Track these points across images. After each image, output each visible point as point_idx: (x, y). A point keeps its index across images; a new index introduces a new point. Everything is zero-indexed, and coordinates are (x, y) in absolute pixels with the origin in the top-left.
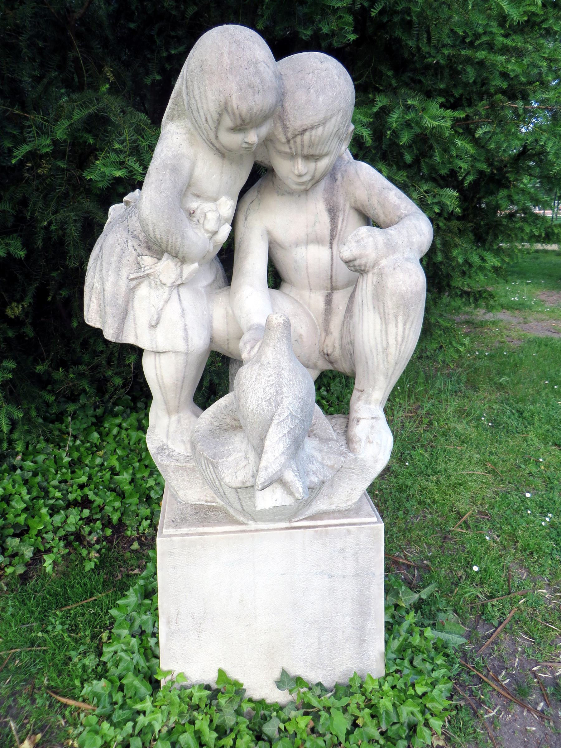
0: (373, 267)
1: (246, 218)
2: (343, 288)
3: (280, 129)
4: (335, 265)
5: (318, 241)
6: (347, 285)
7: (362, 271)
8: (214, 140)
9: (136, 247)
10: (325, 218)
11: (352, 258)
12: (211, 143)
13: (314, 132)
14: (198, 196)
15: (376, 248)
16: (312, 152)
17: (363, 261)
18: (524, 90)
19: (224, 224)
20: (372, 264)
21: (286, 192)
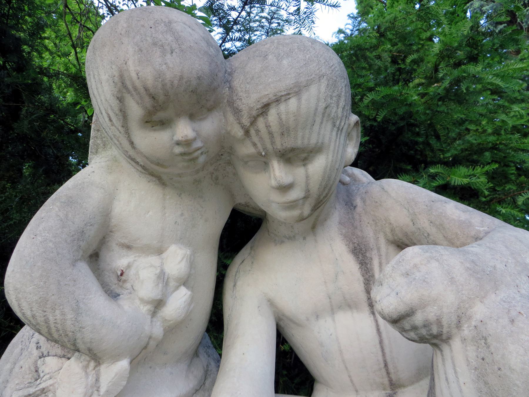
0: (459, 325)
1: (234, 286)
2: (412, 383)
3: (231, 118)
4: (386, 342)
5: (348, 305)
6: (417, 377)
7: (433, 338)
8: (132, 152)
10: (350, 265)
11: (402, 309)
12: (130, 157)
13: (282, 107)
14: (128, 247)
15: (452, 280)
16: (289, 143)
17: (430, 313)
19: (177, 288)
20: (454, 319)
21: (285, 237)
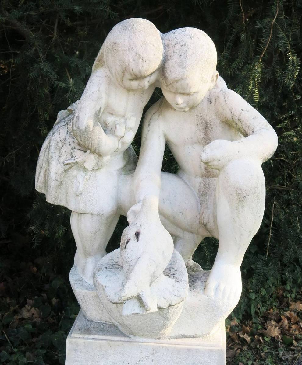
9: (71, 143)
14: (112, 114)
18: (25, 346)
